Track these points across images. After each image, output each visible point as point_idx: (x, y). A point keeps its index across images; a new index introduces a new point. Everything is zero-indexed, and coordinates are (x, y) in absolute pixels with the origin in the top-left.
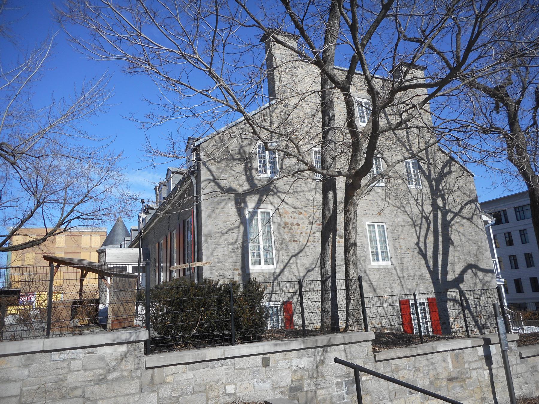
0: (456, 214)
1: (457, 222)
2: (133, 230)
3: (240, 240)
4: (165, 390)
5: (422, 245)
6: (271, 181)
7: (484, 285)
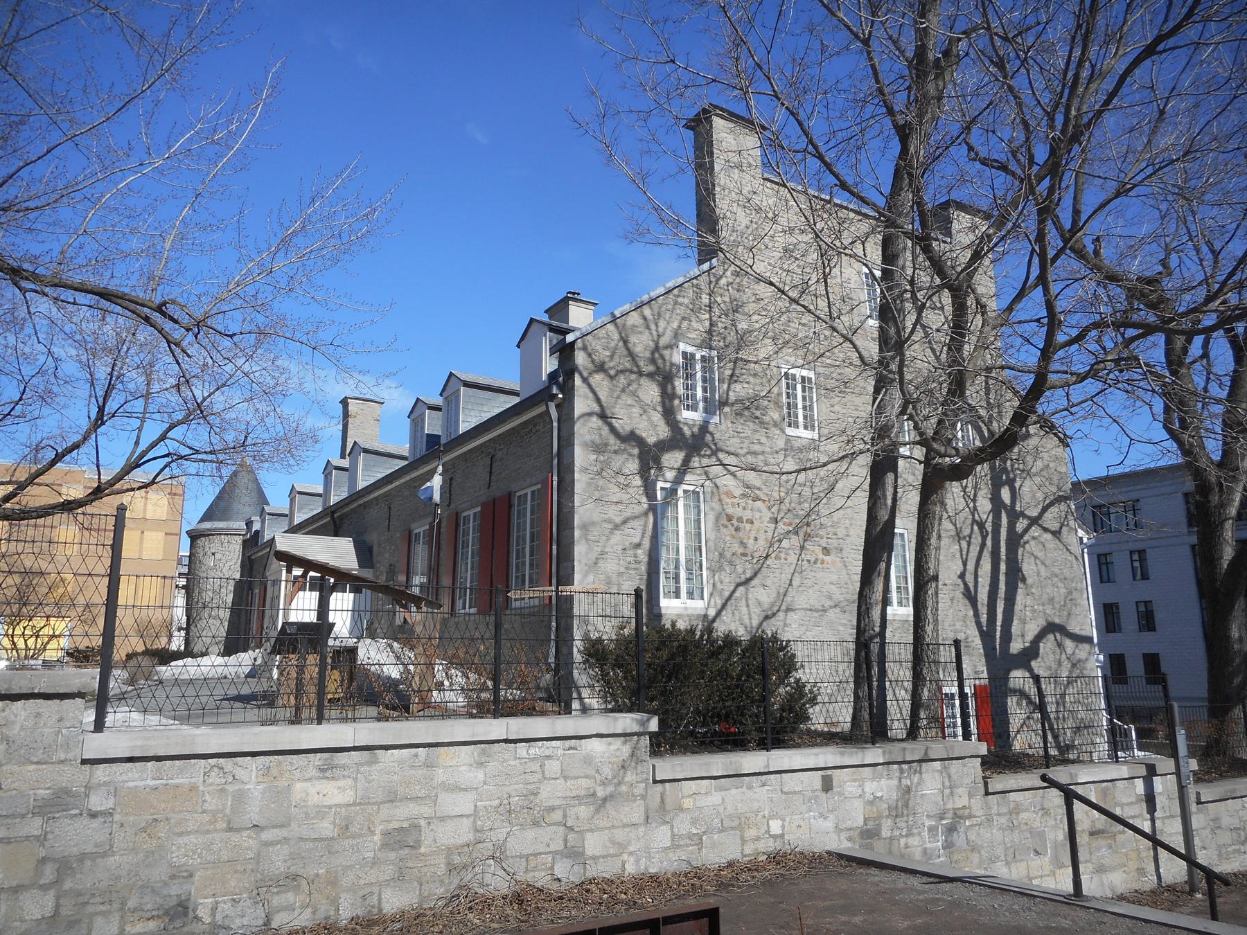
0: (1034, 521)
1: (1034, 538)
2: (300, 493)
3: (646, 544)
4: (682, 822)
5: (969, 578)
6: (704, 428)
7: (1074, 665)
